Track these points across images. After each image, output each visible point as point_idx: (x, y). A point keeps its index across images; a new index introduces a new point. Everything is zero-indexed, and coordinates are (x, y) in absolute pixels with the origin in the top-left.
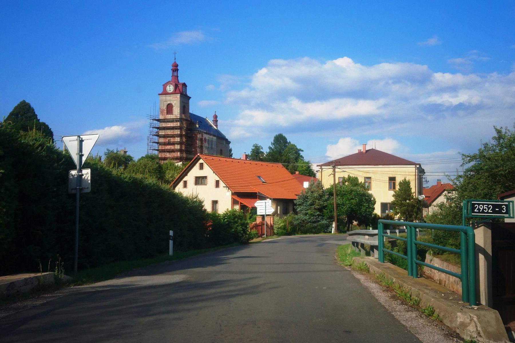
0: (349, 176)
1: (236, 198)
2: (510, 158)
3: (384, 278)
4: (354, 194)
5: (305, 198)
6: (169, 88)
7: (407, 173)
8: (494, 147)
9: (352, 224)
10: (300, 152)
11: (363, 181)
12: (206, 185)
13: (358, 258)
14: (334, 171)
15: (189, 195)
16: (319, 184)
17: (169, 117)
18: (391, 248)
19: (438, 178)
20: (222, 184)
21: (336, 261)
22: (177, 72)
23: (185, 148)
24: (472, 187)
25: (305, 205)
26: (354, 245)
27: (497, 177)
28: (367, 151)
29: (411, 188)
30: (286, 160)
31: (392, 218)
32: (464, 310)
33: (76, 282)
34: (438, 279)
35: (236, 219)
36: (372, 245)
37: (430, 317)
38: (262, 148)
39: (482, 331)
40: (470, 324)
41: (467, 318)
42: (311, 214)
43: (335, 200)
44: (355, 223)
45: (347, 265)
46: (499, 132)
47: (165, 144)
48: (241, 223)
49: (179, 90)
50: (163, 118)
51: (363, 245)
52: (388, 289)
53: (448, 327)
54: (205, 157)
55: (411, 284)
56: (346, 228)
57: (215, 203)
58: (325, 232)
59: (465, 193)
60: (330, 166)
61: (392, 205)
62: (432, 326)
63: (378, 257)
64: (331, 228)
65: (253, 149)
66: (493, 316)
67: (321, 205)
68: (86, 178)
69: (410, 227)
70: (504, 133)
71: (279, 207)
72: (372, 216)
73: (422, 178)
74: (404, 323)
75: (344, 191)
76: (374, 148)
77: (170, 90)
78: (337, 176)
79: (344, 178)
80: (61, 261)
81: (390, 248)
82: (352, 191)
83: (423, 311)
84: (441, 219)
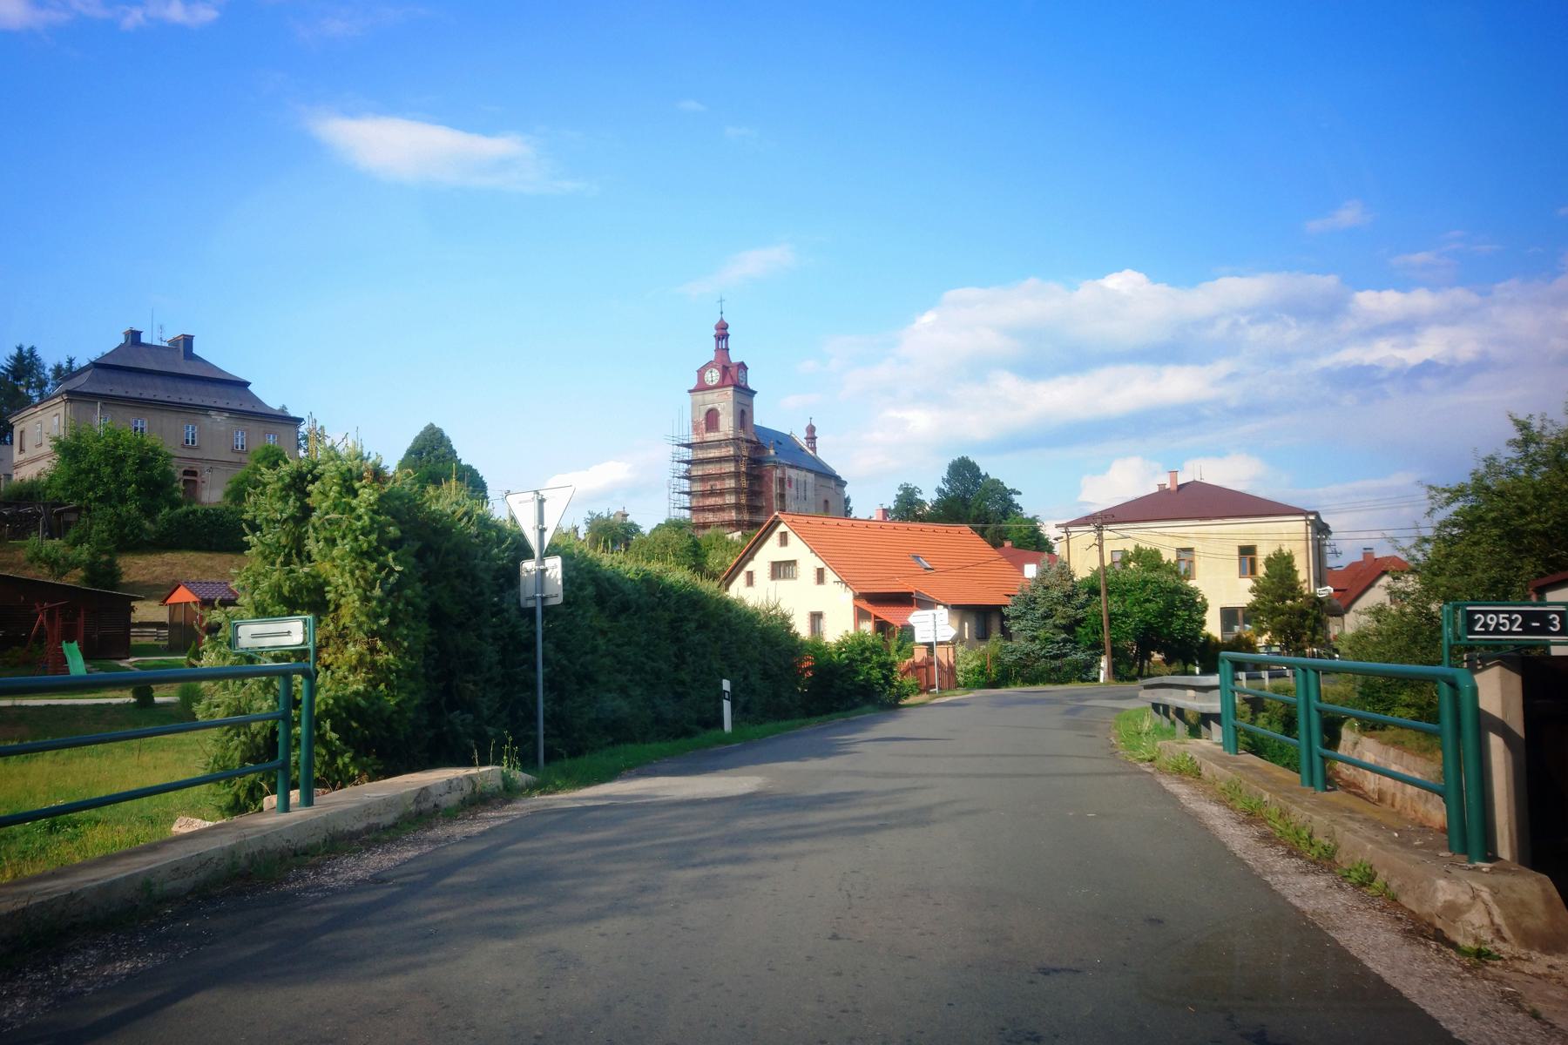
0: (1137, 547)
1: (864, 605)
2: (1557, 490)
3: (1240, 791)
4: (1152, 590)
5: (1031, 602)
7: (1286, 537)
8: (1514, 466)
9: (1150, 660)
10: (1014, 496)
11: (1173, 559)
12: (795, 578)
13: (1170, 742)
14: (1100, 537)
15: (759, 604)
16: (1064, 567)
17: (711, 436)
18: (1252, 714)
19: (1367, 544)
20: (830, 576)
21: (1116, 750)
22: (727, 341)
23: (747, 500)
24: (1459, 566)
25: (1029, 617)
26: (1157, 711)
27: (1525, 538)
28: (1180, 487)
29: (1297, 572)
30: (978, 516)
31: (1250, 647)
32: (1456, 872)
33: (541, 787)
34: (1376, 790)
35: (867, 654)
36: (1205, 711)
37: (1364, 889)
38: (920, 492)
39: (1507, 925)
40: (1470, 906)
41: (1464, 892)
42: (1046, 639)
43: (1105, 605)
44: (1157, 657)
45: (1142, 760)
46: (1523, 426)
47: (704, 494)
48: (878, 662)
49: (732, 378)
50: (698, 441)
51: (1180, 712)
52: (1251, 817)
53: (1413, 912)
54: (791, 518)
55: (1311, 806)
56: (1135, 671)
57: (816, 617)
58: (1083, 681)
59: (1439, 580)
60: (1089, 525)
61: (1250, 613)
62: (1369, 910)
63: (1221, 741)
64: (1097, 670)
65: (900, 495)
66: (1537, 888)
67: (1069, 617)
68: (553, 576)
69: (1305, 670)
70: (1539, 430)
71: (966, 624)
72: (1199, 639)
73: (1325, 545)
74: (1297, 902)
75: (1125, 584)
76: (1198, 479)
78: (1107, 548)
79: (1125, 552)
80: (514, 744)
81: (1249, 716)
82: (1146, 582)
83: (1347, 874)
84: (1379, 643)
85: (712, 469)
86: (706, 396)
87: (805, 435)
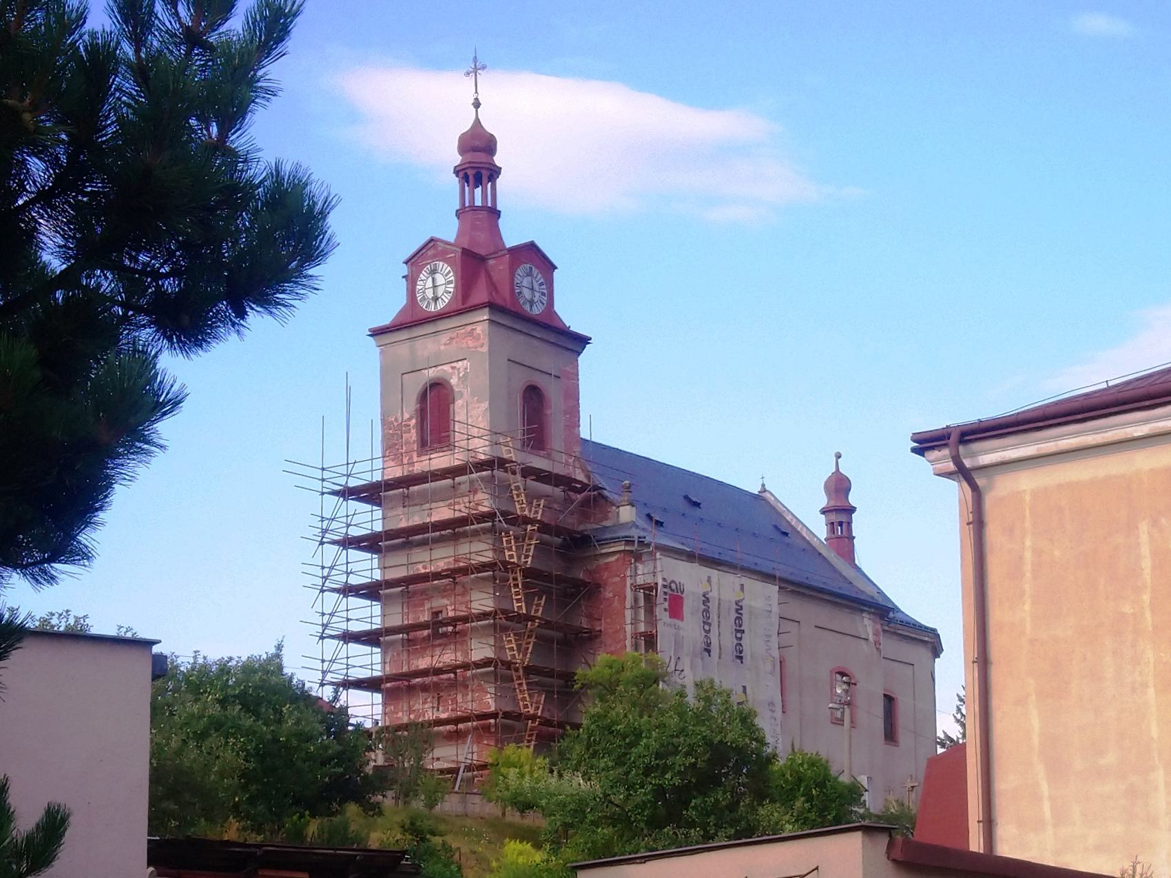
6: (429, 283)
77: (436, 299)
85: (440, 558)
86: (419, 344)
87: (823, 501)
